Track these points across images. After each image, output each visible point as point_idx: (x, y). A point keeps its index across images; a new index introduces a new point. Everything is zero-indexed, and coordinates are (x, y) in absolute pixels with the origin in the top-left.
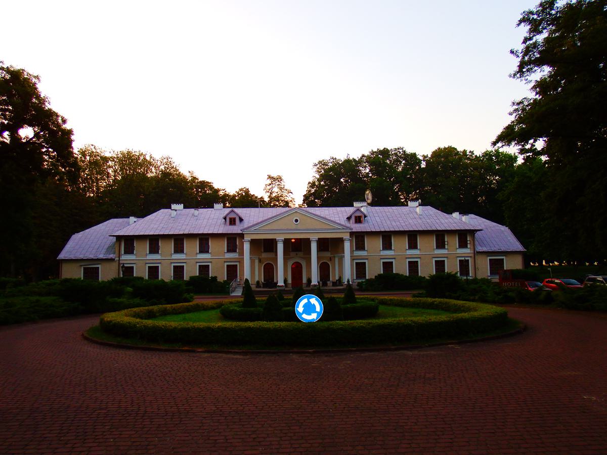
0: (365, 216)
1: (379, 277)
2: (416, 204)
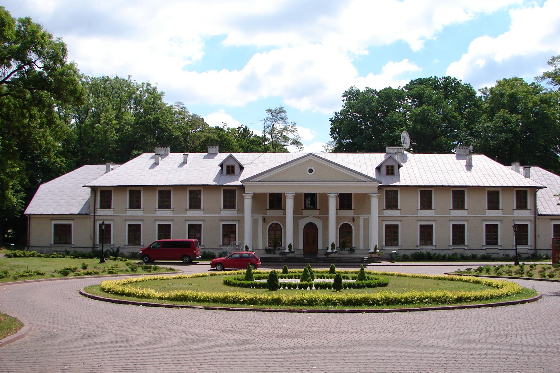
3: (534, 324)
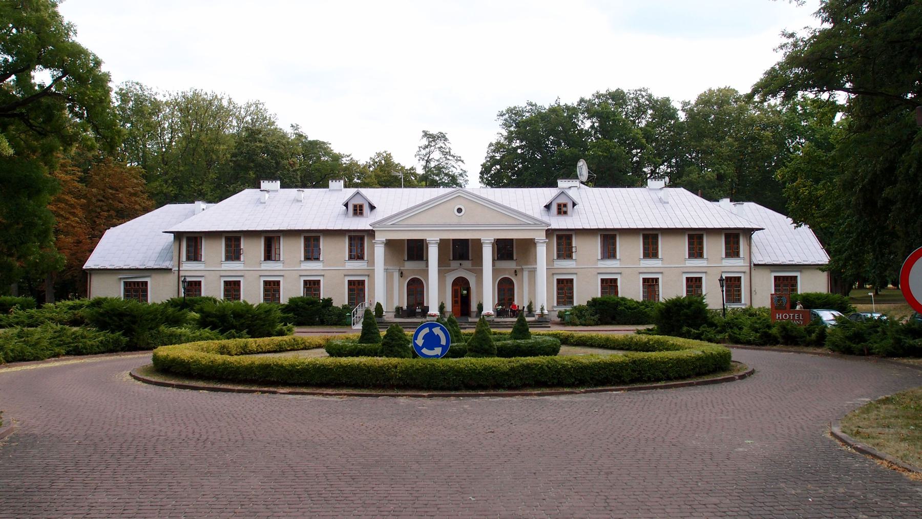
0: (574, 204)
1: (594, 303)
2: (661, 183)
3: (736, 412)
